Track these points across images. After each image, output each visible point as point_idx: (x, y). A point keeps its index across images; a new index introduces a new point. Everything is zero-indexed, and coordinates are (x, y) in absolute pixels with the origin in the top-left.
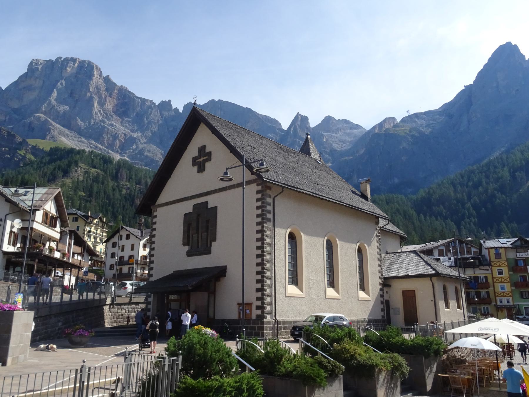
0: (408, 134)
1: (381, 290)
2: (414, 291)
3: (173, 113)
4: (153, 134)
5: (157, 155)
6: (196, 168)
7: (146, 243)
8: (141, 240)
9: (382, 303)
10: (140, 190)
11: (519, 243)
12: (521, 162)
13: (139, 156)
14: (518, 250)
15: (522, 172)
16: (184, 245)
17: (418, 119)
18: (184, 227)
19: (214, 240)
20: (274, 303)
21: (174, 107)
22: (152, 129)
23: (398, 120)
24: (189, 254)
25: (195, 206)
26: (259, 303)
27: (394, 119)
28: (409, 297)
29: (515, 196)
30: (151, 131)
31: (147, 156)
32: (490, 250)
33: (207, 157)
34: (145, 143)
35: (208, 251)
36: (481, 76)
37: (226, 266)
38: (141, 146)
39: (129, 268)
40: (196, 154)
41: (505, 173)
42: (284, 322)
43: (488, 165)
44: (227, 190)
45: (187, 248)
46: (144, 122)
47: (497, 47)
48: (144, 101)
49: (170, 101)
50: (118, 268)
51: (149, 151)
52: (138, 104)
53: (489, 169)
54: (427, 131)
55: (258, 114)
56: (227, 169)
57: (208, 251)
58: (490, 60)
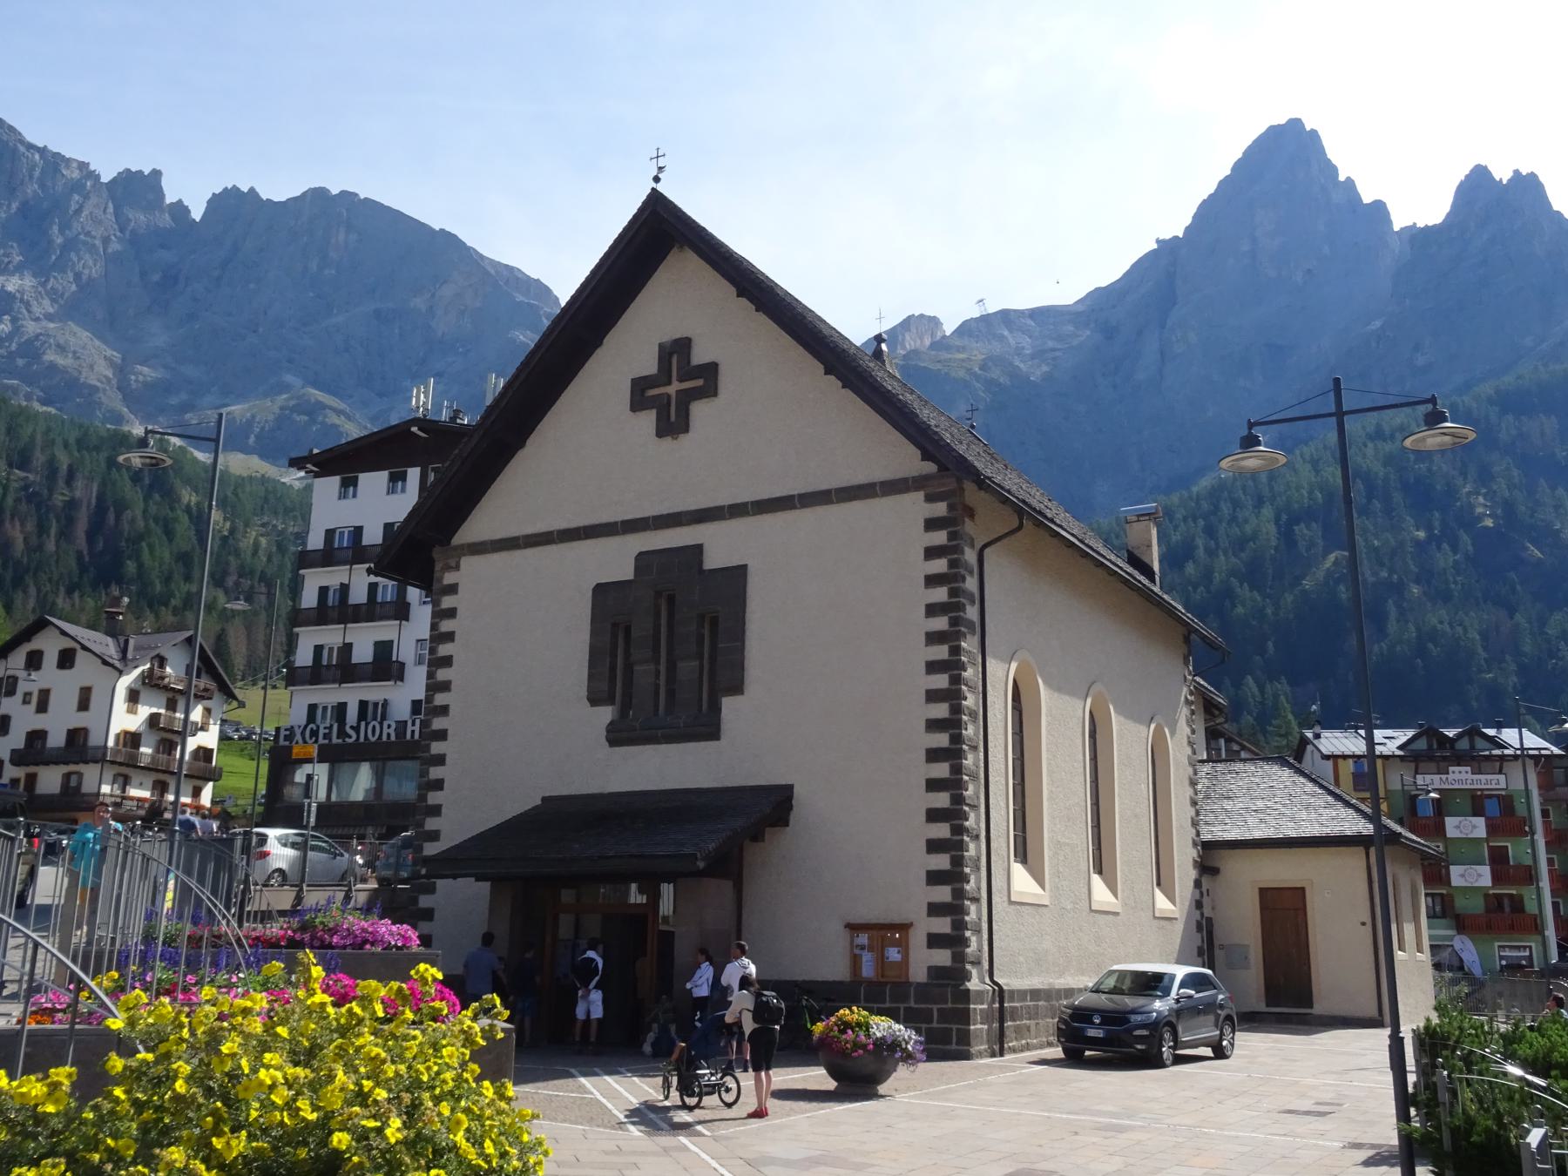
0: (975, 374)
1: (1198, 884)
2: (1303, 889)
3: (166, 221)
4: (81, 288)
5: (91, 367)
6: (648, 419)
7: (138, 686)
8: (121, 673)
9: (1199, 927)
10: (26, 488)
11: (1422, 744)
12: (1311, 492)
13: (20, 362)
14: (1421, 765)
15: (1314, 525)
16: (594, 700)
17: (1011, 331)
18: (593, 633)
19: (737, 687)
20: (985, 926)
21: (170, 198)
22: (79, 267)
23: (949, 328)
24: (618, 736)
25: (643, 560)
26: (943, 925)
27: (934, 322)
28: (1284, 912)
29: (1289, 598)
30: (78, 276)
31: (52, 366)
32: (1340, 761)
33: (700, 382)
34: (50, 317)
35: (707, 728)
36: (1208, 212)
37: (791, 787)
38: (31, 328)
39: (67, 776)
40: (648, 365)
41: (1265, 525)
42: (1022, 994)
43: (1216, 493)
44: (793, 507)
45: (606, 714)
46: (50, 242)
47: (1262, 130)
48: (54, 162)
49: (157, 174)
50: (19, 773)
51: (61, 349)
52: (32, 169)
53: (1217, 508)
54: (1037, 372)
55: (481, 256)
56: (1251, 425)
57: (707, 728)
58: (1238, 166)
